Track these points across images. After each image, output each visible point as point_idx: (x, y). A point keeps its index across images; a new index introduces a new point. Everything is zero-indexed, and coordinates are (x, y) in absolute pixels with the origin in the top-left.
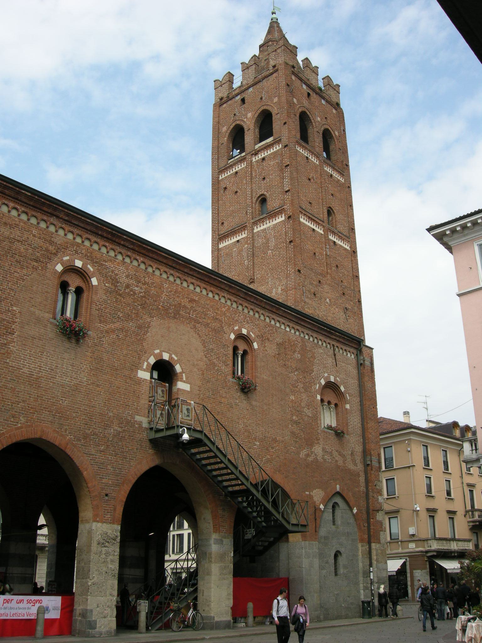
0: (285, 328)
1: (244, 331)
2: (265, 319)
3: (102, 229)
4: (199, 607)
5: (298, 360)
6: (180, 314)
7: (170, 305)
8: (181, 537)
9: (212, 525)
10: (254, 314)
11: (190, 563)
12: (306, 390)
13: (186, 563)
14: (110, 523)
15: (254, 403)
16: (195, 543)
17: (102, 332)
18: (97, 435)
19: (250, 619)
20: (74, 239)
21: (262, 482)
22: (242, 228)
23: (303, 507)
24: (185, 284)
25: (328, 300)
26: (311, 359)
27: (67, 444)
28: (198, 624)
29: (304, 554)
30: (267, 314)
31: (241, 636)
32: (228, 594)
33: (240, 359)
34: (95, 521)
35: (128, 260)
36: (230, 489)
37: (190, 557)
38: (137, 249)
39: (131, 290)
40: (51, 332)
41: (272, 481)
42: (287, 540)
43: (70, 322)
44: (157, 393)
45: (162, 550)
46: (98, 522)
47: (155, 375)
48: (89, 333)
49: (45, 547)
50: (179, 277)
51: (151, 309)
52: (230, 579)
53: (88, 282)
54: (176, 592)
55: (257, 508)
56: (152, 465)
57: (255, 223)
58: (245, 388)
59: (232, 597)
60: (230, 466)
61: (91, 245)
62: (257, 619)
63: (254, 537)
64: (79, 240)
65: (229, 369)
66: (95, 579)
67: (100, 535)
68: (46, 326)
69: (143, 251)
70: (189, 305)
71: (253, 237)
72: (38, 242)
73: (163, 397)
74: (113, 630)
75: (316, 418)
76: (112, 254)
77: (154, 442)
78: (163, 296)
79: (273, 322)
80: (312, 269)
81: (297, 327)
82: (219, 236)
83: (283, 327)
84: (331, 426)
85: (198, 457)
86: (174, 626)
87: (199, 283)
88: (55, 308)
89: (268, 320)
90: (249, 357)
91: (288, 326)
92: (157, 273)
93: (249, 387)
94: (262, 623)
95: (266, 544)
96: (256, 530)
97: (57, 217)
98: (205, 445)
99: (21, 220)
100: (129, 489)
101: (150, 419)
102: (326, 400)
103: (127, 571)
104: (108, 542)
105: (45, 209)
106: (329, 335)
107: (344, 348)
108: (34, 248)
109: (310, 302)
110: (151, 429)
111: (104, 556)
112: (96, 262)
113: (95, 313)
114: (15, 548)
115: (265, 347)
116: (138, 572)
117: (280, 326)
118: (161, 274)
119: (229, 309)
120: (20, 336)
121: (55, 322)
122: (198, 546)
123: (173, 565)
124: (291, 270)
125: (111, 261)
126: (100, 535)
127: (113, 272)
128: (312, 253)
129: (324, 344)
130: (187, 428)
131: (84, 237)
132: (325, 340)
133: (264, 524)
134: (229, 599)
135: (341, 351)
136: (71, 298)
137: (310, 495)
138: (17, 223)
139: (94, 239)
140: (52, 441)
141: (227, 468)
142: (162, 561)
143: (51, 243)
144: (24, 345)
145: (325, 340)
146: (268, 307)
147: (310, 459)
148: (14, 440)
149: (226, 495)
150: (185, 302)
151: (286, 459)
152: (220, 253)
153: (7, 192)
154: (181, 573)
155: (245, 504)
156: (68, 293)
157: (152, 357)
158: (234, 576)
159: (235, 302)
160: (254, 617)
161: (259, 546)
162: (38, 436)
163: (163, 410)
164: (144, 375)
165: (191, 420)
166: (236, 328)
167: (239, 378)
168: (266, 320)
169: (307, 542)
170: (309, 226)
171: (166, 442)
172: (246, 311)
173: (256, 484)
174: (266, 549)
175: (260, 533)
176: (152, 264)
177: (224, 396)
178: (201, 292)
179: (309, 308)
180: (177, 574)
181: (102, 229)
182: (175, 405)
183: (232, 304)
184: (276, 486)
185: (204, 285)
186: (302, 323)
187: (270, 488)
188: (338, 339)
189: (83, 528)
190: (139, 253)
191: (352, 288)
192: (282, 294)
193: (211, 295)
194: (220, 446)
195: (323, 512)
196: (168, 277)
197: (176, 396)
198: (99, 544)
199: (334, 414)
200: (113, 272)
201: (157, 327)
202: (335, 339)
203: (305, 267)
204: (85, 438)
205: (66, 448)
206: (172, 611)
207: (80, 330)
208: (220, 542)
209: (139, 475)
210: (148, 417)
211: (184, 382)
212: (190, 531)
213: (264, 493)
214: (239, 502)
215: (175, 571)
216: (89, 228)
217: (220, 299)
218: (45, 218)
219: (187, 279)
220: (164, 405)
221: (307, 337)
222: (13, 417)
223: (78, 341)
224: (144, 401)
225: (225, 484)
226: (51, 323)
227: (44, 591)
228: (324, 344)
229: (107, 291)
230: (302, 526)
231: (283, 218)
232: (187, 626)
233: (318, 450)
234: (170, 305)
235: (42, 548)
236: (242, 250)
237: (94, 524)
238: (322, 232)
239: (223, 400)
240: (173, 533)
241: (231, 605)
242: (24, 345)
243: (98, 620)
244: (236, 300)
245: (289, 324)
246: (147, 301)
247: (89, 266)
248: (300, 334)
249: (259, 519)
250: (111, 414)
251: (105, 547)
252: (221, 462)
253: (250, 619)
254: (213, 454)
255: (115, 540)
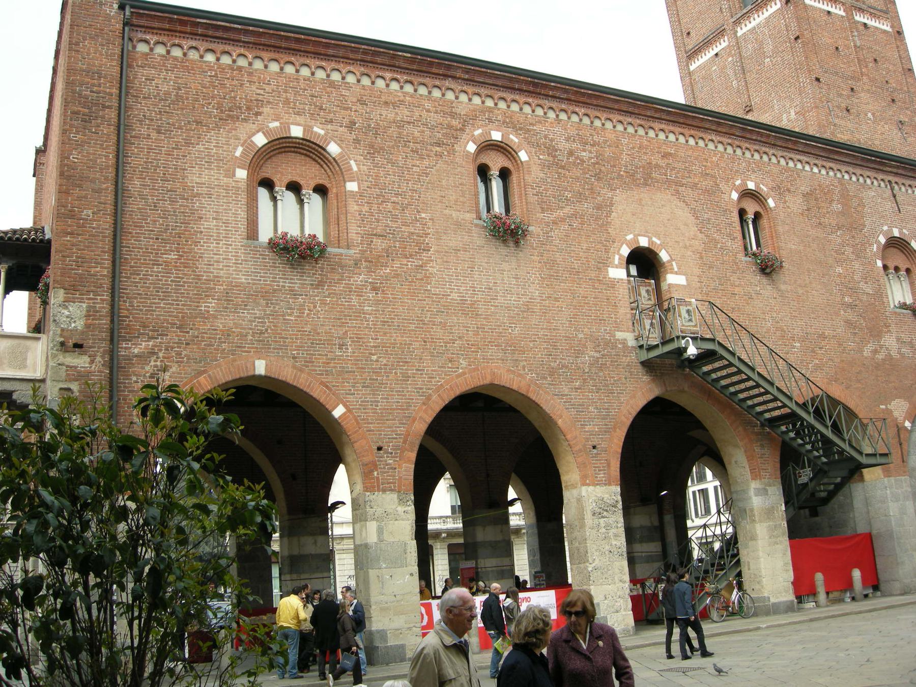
0: (812, 169)
1: (751, 185)
2: (779, 162)
3: (518, 81)
4: (746, 586)
5: (840, 212)
6: (652, 178)
7: (636, 167)
8: (704, 492)
9: (748, 469)
10: (761, 157)
11: (724, 527)
12: (858, 257)
13: (718, 528)
14: (605, 484)
15: (783, 287)
16: (726, 498)
17: (547, 224)
18: (567, 367)
19: (822, 596)
20: (483, 102)
21: (813, 400)
22: (719, 33)
23: (879, 428)
24: (652, 134)
25: (869, 115)
26: (859, 209)
27: (529, 386)
28: (748, 608)
29: (889, 496)
30: (780, 153)
31: (811, 620)
32: (785, 564)
33: (751, 226)
34: (584, 484)
35: (563, 116)
36: (767, 415)
37: (723, 519)
38: (573, 98)
39: (577, 158)
40: (479, 238)
41: (828, 396)
42: (862, 479)
43: (501, 219)
44: (640, 295)
45: (681, 516)
46: (588, 485)
47: (633, 270)
48: (530, 228)
49: (521, 529)
50: (641, 125)
51: (611, 178)
52: (784, 543)
53: (514, 158)
54: (710, 569)
55: (810, 438)
56: (651, 397)
57: (737, 22)
58: (767, 267)
59: (791, 568)
60: (762, 382)
61: (509, 107)
62: (831, 596)
63: (811, 480)
64: (489, 103)
65: (739, 243)
66: (597, 562)
67: (594, 503)
68: (469, 231)
69: (582, 99)
70: (662, 163)
71: (737, 43)
72: (434, 118)
73: (650, 299)
74: (630, 628)
75: (880, 295)
76: (539, 112)
77: (647, 365)
78: (624, 157)
79: (791, 164)
80: (837, 73)
81: (828, 164)
82: (688, 55)
83: (807, 168)
84: (905, 304)
85: (714, 376)
86: (714, 614)
87: (672, 128)
88: (477, 204)
89: (783, 162)
90: (764, 222)
91: (815, 165)
92: (609, 125)
93: (772, 265)
94: (841, 600)
95: (832, 487)
96: (813, 470)
97: (454, 77)
98: (722, 358)
99: (405, 93)
100: (624, 434)
101: (636, 334)
102: (891, 265)
103: (638, 547)
104: (606, 511)
105: (434, 70)
106: (881, 168)
107: (908, 182)
108: (432, 129)
109: (842, 123)
110: (641, 347)
111: (604, 530)
112: (521, 129)
113: (533, 199)
114: (483, 534)
115: (785, 202)
116: (653, 547)
117: (804, 167)
118: (614, 127)
119: (722, 157)
120: (438, 251)
121: (481, 222)
122: (732, 501)
123: (700, 533)
124: (805, 79)
125: (540, 122)
126: (594, 503)
127: (546, 137)
128: (833, 49)
129: (876, 183)
130: (691, 338)
131: (496, 97)
132: (876, 176)
133: (824, 460)
134: (787, 570)
135: (903, 189)
136: (496, 186)
137: (887, 409)
138: (402, 98)
139: (509, 96)
140: (507, 385)
141: (758, 386)
142: (682, 530)
143: (453, 115)
144: (447, 262)
145: (876, 176)
146: (779, 143)
147: (880, 356)
148: (458, 392)
149: (762, 425)
150: (656, 159)
151: (843, 361)
152: (693, 77)
153: (379, 60)
154: (712, 542)
155: (792, 435)
156: (490, 180)
157: (624, 246)
158: (790, 537)
159: (729, 144)
160: (828, 593)
161: (821, 491)
162: (487, 381)
163: (653, 317)
164: (618, 273)
165: (696, 326)
166: (738, 182)
167: (754, 254)
168: (779, 163)
169: (892, 479)
170: (820, 9)
171: (666, 362)
172: (748, 154)
173: (804, 404)
174: (832, 494)
175: (819, 473)
176: (598, 114)
177: (737, 283)
178: (677, 139)
179: (842, 133)
180: (706, 545)
181: (518, 81)
182: (669, 309)
183: (725, 149)
184: (834, 402)
185: (680, 130)
186: (836, 157)
187: (825, 408)
188: (895, 170)
189: (568, 496)
190: (578, 103)
191: (906, 88)
192: (797, 120)
193: (692, 142)
194: (744, 357)
195: (911, 432)
196: (625, 129)
197: (668, 296)
198: (594, 514)
199: (906, 285)
200: (546, 137)
201: (624, 204)
202: (891, 172)
203: (826, 72)
204: (551, 375)
205: (528, 391)
206: (708, 594)
207: (517, 227)
208: (763, 492)
209: (634, 413)
210: (634, 331)
211: (676, 273)
212: (717, 483)
213: (818, 414)
214: (783, 433)
215: (704, 541)
216: (499, 83)
217: (706, 145)
218: (437, 83)
219: (652, 125)
220: (653, 311)
221: (846, 177)
222: (450, 361)
223: (517, 243)
224: (624, 311)
225: (759, 409)
226: (476, 226)
227: (528, 586)
228: (876, 183)
229: (543, 166)
230: (881, 455)
231: (779, 5)
232: (733, 614)
233: (890, 341)
234: (636, 167)
235: (517, 531)
236: (725, 67)
237: (584, 488)
238: (842, 13)
239: (737, 290)
240: (692, 488)
241: (792, 579)
242: (447, 262)
243: (609, 617)
244: (730, 141)
245: (816, 162)
246: (603, 168)
247: (511, 136)
248: (835, 174)
249: (816, 454)
250: (581, 336)
251: (603, 517)
252: (749, 379)
253: (822, 596)
254: (735, 370)
255: (615, 506)
